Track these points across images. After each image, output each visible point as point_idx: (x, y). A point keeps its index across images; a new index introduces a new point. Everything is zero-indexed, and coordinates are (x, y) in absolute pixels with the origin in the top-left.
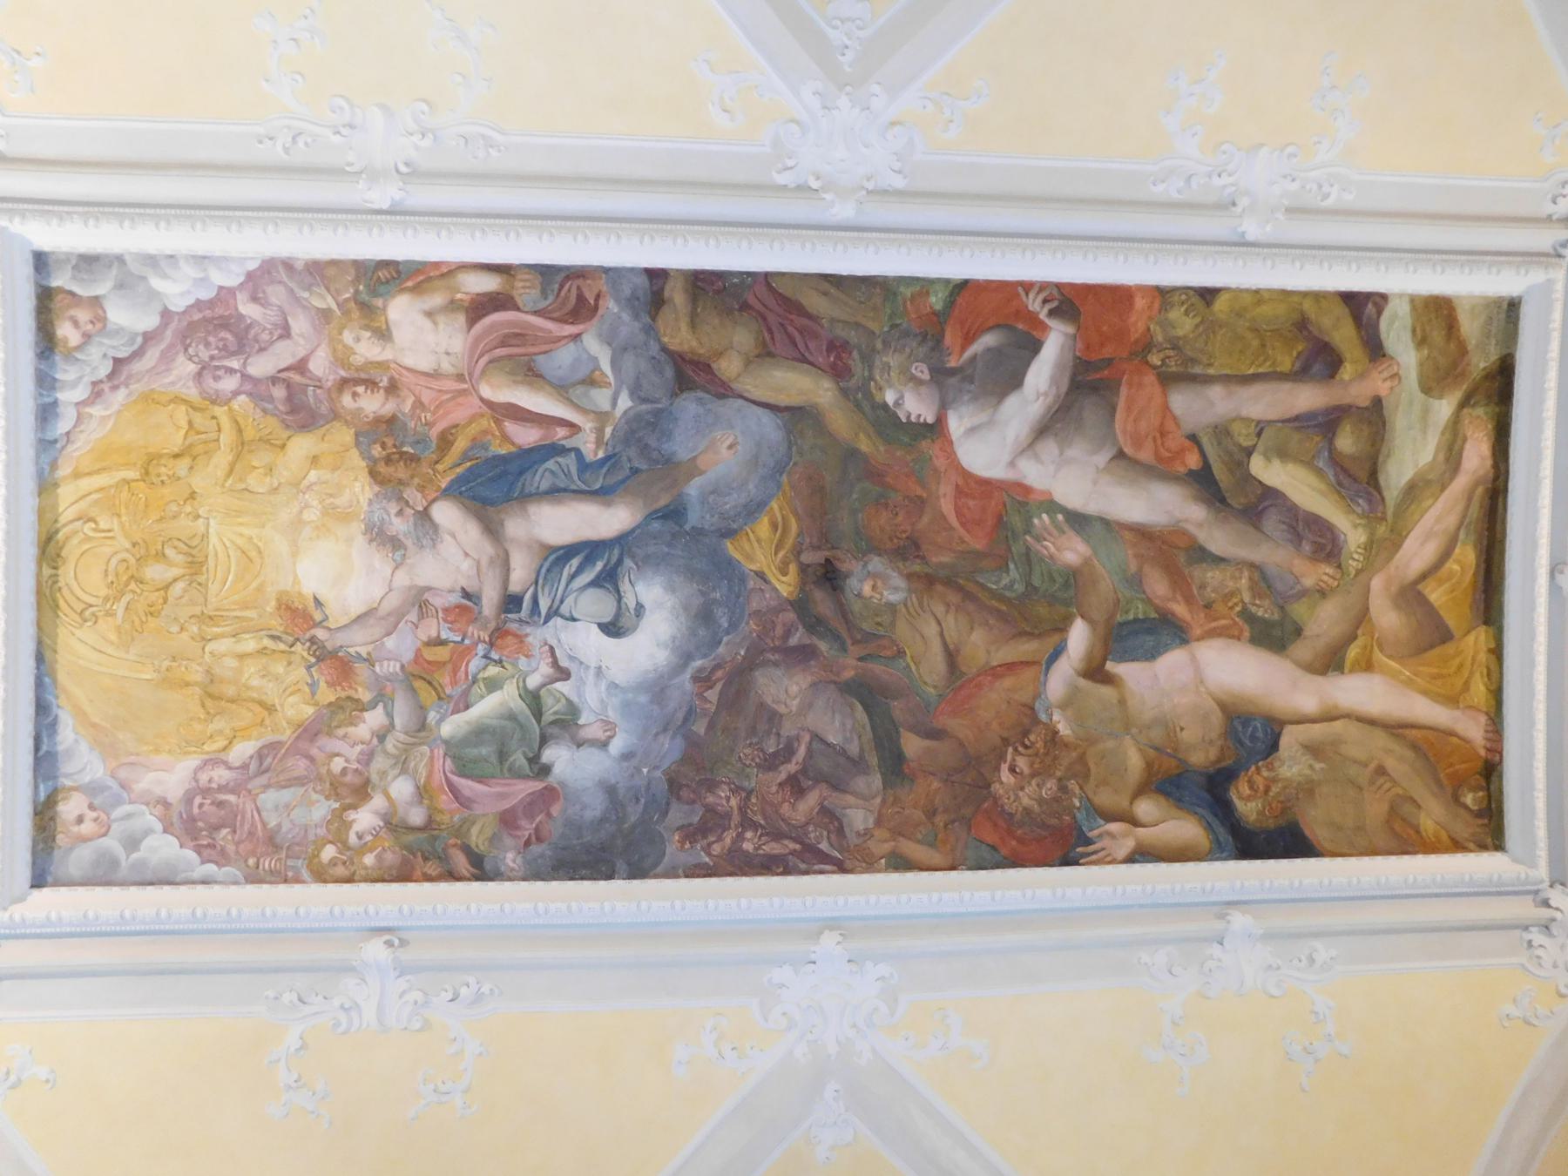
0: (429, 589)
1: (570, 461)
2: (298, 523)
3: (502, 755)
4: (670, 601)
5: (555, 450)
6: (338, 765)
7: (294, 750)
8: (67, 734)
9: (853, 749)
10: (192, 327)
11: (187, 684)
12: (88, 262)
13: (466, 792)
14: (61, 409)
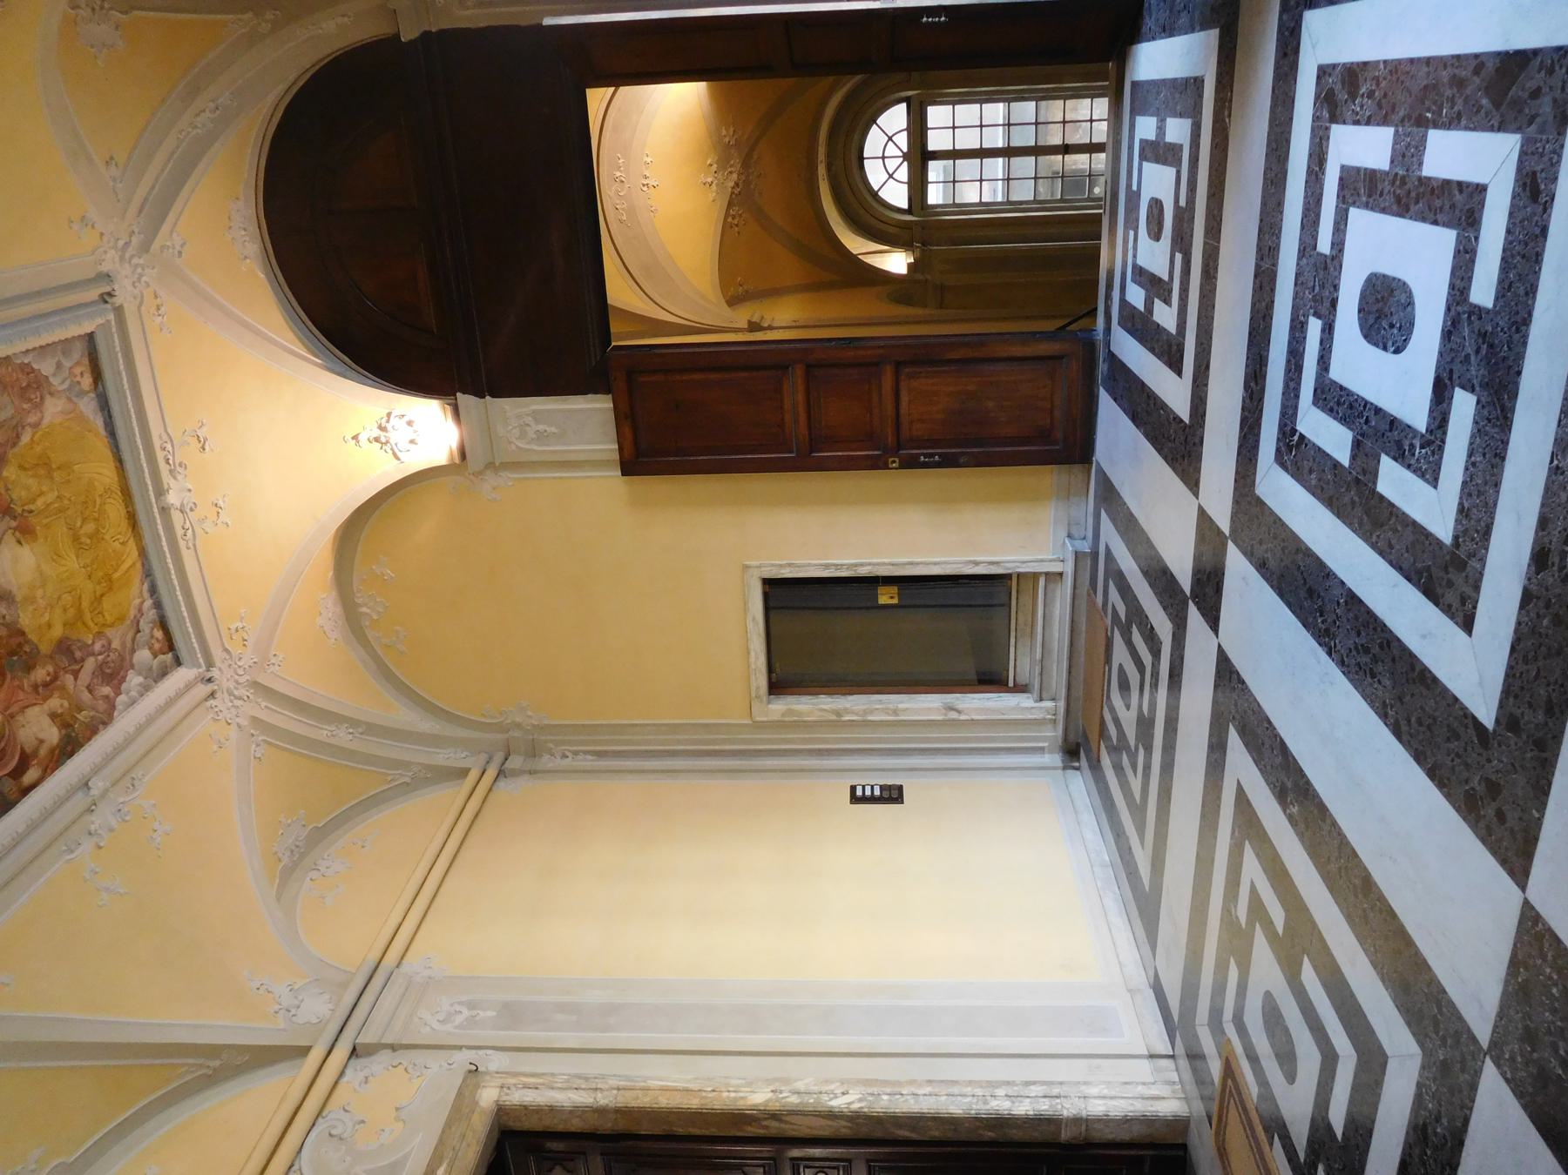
8: (99, 422)
13: (1302, 427)
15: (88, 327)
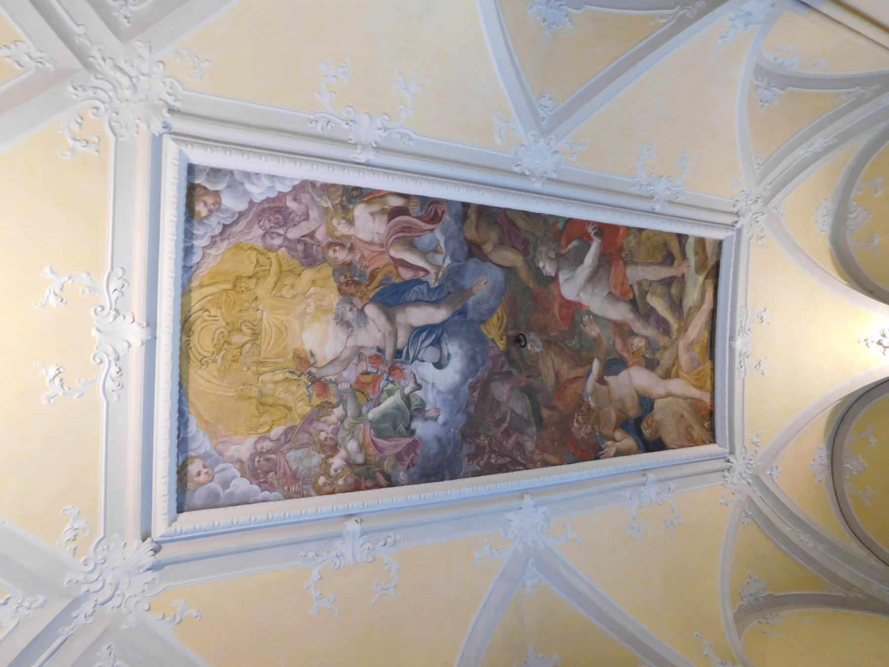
0: (363, 347)
1: (423, 287)
2: (304, 314)
3: (395, 427)
4: (460, 352)
5: (418, 282)
6: (323, 435)
7: (302, 430)
8: (193, 427)
9: (526, 416)
10: (264, 211)
11: (250, 398)
12: (215, 173)
13: (381, 445)
14: (195, 250)
15: (189, 521)
